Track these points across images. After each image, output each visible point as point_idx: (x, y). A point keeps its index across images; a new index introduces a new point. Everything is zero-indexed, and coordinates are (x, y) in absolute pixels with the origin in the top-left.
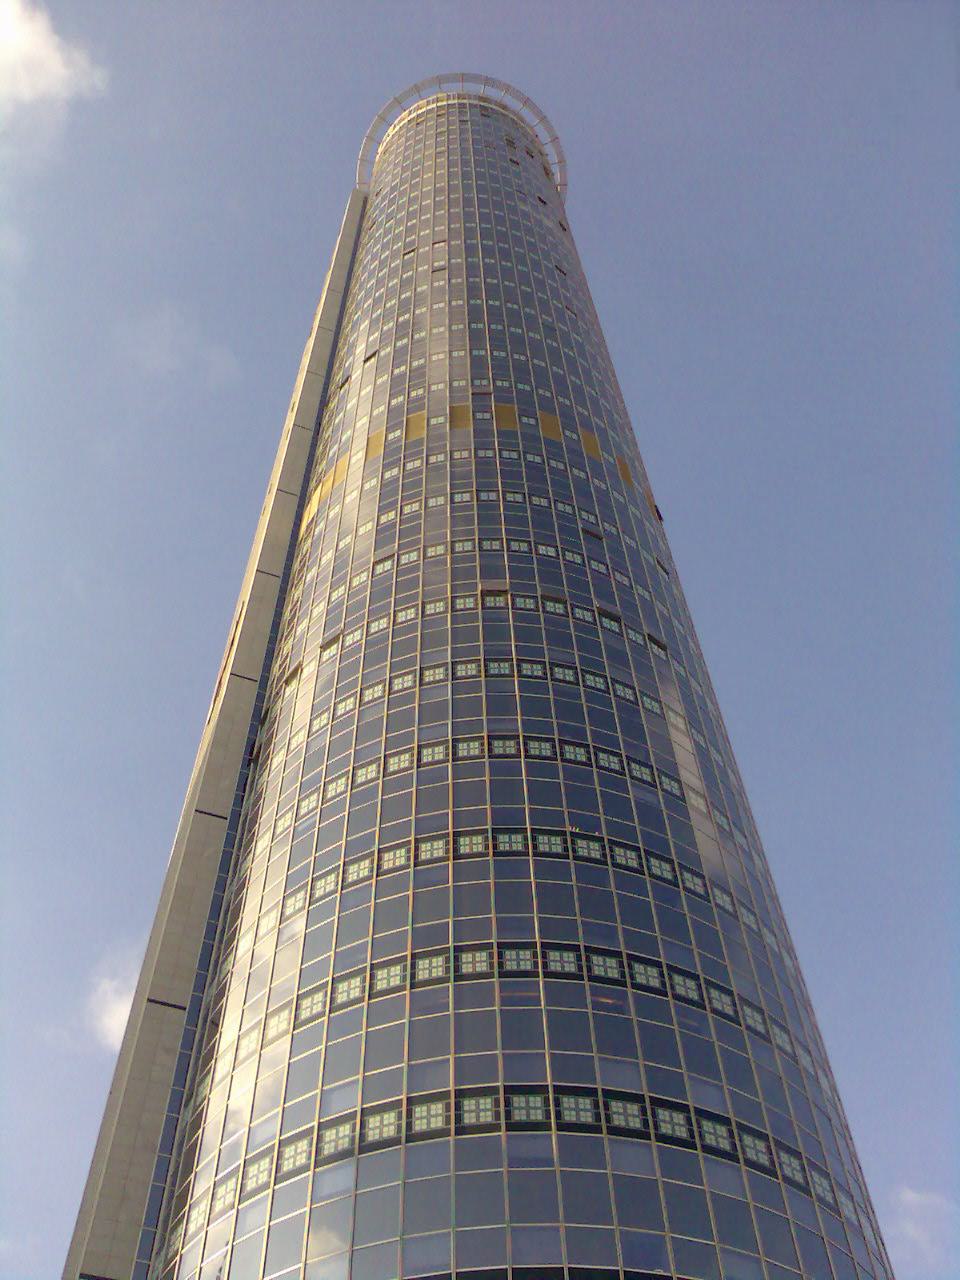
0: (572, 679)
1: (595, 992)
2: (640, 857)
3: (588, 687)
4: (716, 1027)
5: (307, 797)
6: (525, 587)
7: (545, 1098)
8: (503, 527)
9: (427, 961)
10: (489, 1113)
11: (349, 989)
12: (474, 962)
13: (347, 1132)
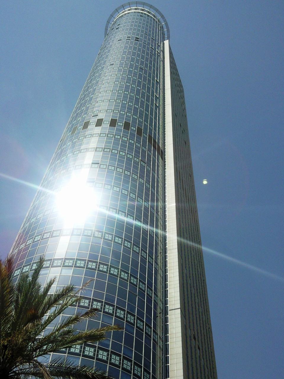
0: (129, 175)
1: (108, 346)
2: (131, 245)
3: (134, 141)
4: (134, 353)
5: (70, 154)
6: (125, 135)
7: (102, 304)
8: (119, 147)
9: (80, 262)
10: (87, 304)
11: (58, 263)
12: (92, 265)
13: (60, 262)
